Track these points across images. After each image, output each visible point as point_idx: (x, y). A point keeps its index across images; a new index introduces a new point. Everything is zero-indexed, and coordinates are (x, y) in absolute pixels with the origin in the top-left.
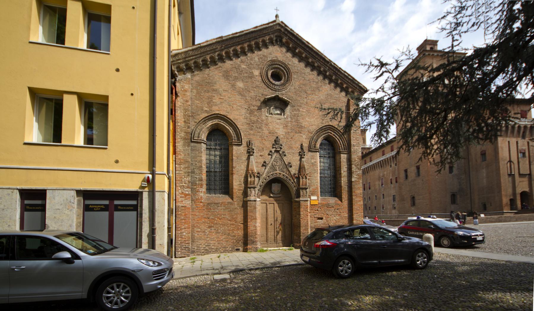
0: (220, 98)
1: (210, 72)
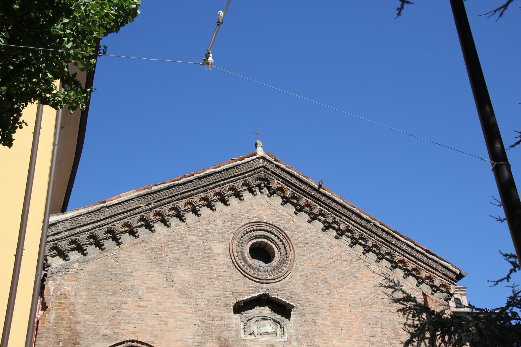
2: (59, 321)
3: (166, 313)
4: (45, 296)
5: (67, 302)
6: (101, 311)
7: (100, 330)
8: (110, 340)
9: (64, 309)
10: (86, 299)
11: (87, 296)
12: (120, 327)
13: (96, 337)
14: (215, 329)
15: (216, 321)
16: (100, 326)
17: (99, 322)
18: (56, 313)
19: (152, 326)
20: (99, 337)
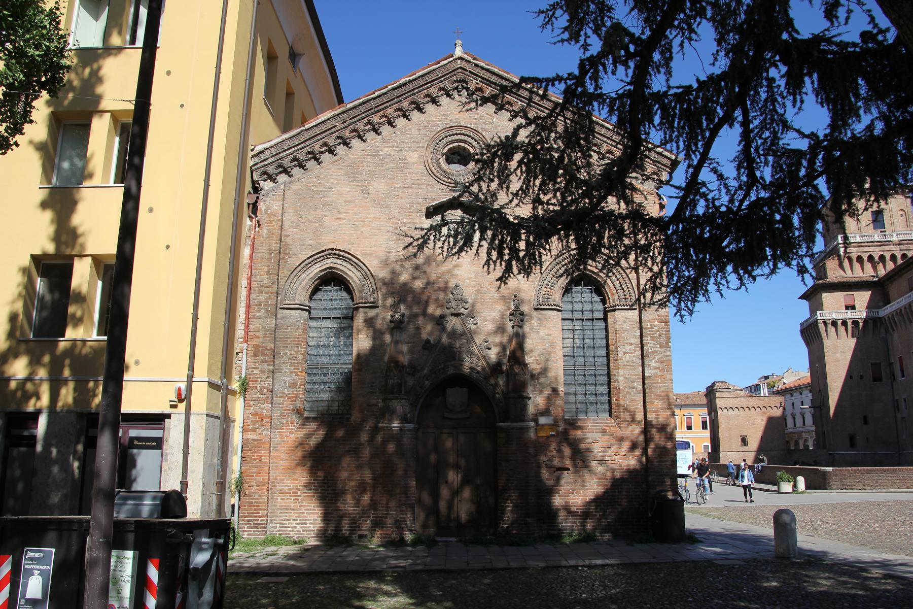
0: (338, 218)
1: (322, 170)
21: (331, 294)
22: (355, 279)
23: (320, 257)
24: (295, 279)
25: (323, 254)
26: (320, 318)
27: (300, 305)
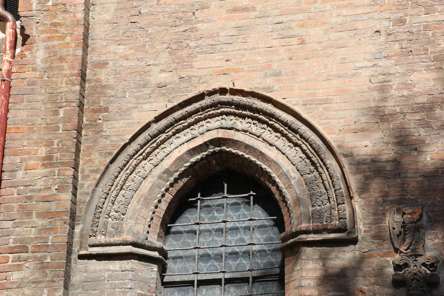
2: (55, 65)
3: (301, 16)
4: (21, 14)
5: (69, 20)
6: (150, 34)
7: (150, 76)
8: (173, 95)
9: (63, 38)
10: (116, 10)
11: (118, 3)
12: (194, 63)
13: (141, 91)
14: (433, 34)
15: (437, 14)
16: (149, 67)
17: (146, 59)
18: (47, 48)
19: (266, 51)
20: (149, 92)
21: (220, 216)
22: (286, 166)
23: (190, 115)
24: (123, 175)
25: (197, 105)
26: (190, 283)
27: (135, 244)
